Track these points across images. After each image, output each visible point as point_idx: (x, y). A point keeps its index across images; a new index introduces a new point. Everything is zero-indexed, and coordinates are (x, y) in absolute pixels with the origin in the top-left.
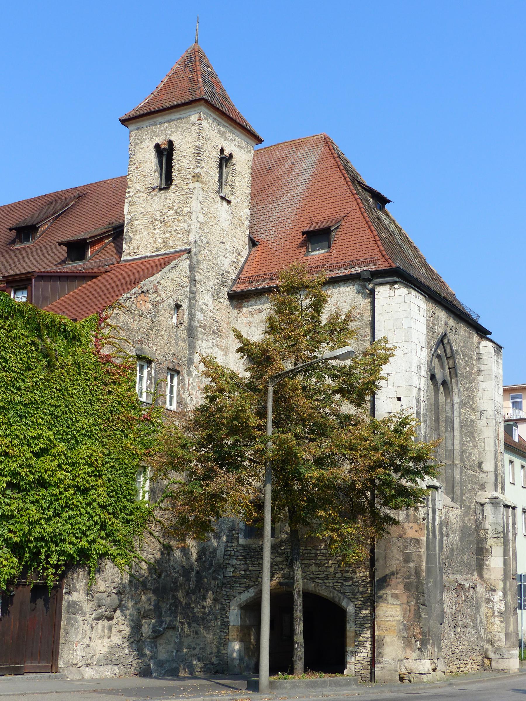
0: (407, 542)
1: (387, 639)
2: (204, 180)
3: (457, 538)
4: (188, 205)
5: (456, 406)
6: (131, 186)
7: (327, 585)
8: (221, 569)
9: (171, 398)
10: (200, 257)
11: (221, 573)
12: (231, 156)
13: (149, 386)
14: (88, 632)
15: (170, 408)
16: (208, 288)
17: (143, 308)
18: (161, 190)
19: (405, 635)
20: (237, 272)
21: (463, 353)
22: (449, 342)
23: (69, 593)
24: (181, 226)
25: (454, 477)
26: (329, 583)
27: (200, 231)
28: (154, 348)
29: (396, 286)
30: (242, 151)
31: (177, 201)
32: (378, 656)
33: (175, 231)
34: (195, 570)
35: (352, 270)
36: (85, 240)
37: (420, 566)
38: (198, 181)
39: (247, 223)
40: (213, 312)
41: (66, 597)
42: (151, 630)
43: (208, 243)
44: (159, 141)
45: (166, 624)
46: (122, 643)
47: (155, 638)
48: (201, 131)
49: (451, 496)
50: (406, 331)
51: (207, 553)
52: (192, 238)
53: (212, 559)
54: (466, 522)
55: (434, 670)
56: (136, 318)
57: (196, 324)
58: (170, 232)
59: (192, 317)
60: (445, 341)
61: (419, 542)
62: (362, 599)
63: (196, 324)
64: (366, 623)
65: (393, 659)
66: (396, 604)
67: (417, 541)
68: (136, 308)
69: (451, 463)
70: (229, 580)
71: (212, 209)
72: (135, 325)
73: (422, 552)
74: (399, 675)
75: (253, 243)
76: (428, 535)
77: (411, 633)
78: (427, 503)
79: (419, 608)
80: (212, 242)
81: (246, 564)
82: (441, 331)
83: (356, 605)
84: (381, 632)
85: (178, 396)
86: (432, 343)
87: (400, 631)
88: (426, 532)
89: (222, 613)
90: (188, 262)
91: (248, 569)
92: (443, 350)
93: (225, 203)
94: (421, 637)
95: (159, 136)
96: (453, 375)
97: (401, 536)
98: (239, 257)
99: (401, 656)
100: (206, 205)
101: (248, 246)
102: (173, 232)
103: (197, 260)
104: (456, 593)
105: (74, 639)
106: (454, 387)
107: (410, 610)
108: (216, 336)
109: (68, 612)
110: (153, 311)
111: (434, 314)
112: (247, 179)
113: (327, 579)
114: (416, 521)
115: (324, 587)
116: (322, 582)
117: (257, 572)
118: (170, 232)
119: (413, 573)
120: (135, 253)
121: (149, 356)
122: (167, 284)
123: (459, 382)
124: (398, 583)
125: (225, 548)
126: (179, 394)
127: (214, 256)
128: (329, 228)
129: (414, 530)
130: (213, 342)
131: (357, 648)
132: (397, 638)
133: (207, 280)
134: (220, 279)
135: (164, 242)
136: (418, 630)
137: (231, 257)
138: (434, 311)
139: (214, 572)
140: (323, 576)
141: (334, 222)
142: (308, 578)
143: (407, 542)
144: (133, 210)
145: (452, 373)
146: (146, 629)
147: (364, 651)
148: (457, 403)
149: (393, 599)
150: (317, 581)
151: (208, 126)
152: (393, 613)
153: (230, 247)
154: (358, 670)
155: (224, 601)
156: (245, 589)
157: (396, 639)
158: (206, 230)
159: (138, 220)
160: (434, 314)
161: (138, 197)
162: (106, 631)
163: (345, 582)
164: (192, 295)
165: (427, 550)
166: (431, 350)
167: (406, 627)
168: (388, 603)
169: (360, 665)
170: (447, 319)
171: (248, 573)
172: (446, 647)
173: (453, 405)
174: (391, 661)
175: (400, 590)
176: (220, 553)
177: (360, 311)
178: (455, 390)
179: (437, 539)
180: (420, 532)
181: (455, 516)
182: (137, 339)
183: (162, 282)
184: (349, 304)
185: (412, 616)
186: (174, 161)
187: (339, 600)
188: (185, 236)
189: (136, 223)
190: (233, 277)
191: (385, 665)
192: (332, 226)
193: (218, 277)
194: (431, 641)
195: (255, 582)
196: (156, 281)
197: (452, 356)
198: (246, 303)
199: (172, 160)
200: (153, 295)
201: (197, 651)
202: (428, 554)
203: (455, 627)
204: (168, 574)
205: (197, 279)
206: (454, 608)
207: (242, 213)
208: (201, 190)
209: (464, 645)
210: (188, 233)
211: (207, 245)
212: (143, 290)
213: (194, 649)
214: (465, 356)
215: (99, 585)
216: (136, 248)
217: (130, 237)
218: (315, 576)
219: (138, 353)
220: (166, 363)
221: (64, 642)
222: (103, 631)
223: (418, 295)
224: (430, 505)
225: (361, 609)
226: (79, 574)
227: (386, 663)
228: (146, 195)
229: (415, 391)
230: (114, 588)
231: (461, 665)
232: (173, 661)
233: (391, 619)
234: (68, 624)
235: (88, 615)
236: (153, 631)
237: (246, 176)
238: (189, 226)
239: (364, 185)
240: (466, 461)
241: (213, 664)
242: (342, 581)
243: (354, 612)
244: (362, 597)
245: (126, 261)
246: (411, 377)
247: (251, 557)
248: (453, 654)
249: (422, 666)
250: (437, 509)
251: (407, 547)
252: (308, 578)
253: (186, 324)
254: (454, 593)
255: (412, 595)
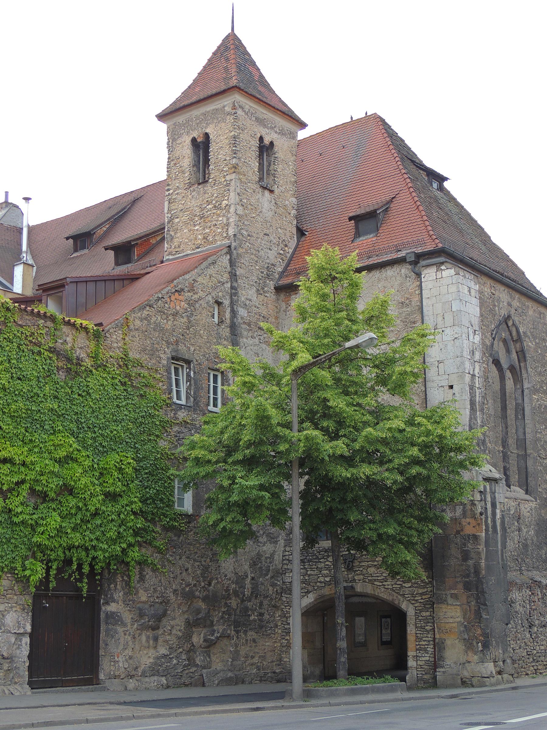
0: (465, 540)
1: (448, 642)
2: (242, 170)
3: (532, 532)
4: (226, 198)
5: (526, 392)
6: (170, 183)
7: (386, 587)
8: (279, 575)
9: (215, 399)
10: (241, 251)
11: (279, 579)
12: (272, 143)
13: (189, 388)
14: (130, 643)
15: (214, 409)
16: (252, 283)
17: (178, 308)
18: (199, 184)
19: (466, 637)
20: (284, 265)
21: (533, 335)
22: (513, 324)
23: (107, 603)
24: (220, 221)
25: (526, 468)
26: (388, 585)
27: (239, 223)
28: (192, 349)
29: (443, 267)
30: (285, 138)
31: (215, 195)
32: (439, 660)
33: (214, 226)
34: (249, 577)
35: (399, 253)
36: (129, 242)
37: (479, 564)
38: (234, 172)
39: (294, 212)
40: (258, 308)
41: (103, 608)
42: (202, 640)
43: (249, 235)
44: (195, 134)
45: (218, 632)
46: (169, 653)
47: (208, 647)
48: (236, 120)
49: (525, 488)
50: (455, 315)
51: (263, 558)
52: (231, 232)
53: (269, 564)
54: (543, 515)
55: (500, 673)
56: (170, 318)
57: (239, 321)
58: (210, 227)
59: (234, 313)
60: (510, 323)
61: (477, 539)
62: (422, 601)
63: (239, 321)
64: (427, 626)
65: (455, 663)
66: (456, 605)
67: (476, 538)
68: (169, 308)
69: (523, 453)
70: (288, 586)
71: (253, 201)
72: (169, 325)
73: (481, 549)
74: (462, 679)
75: (301, 232)
76: (487, 530)
77: (472, 634)
78: (485, 497)
79: (479, 608)
80: (254, 235)
81: (305, 568)
82: (504, 312)
83: (416, 607)
84: (442, 634)
85: (222, 397)
86: (493, 326)
87: (461, 633)
88: (484, 527)
89: (283, 619)
90: (228, 257)
91: (307, 574)
92: (508, 333)
93: (267, 193)
94: (483, 639)
95: (195, 129)
96: (522, 359)
97: (458, 532)
98: (286, 248)
99: (463, 659)
100: (245, 196)
101: (295, 236)
102: (212, 227)
103: (237, 254)
104: (530, 591)
105: (115, 650)
106: (523, 372)
107: (470, 610)
108: (262, 332)
109: (107, 623)
110: (189, 310)
111: (494, 295)
112: (291, 167)
113: (386, 581)
114: (474, 517)
115: (383, 590)
116: (381, 584)
117: (316, 577)
118: (210, 227)
119: (472, 571)
120: (177, 252)
121: (187, 358)
122: (204, 282)
123: (528, 366)
124: (457, 582)
125: (283, 553)
126: (223, 394)
127: (257, 249)
128: (375, 211)
129: (472, 525)
130: (260, 339)
131: (418, 652)
132: (458, 640)
133: (249, 273)
134: (265, 273)
135: (204, 238)
136: (479, 632)
137: (276, 249)
138: (494, 292)
139: (272, 577)
140: (382, 577)
141: (380, 205)
142: (367, 581)
143: (465, 540)
144: (173, 207)
145: (520, 356)
146: (197, 639)
147: (426, 655)
148: (528, 388)
149: (452, 600)
150: (376, 583)
151: (243, 114)
152: (453, 614)
153: (274, 238)
154: (421, 675)
155: (284, 607)
156: (304, 594)
157: (457, 642)
158: (245, 222)
159: (178, 218)
160: (494, 295)
161: (177, 194)
162: (151, 642)
163: (404, 583)
164: (233, 291)
165: (485, 547)
166: (492, 334)
167: (467, 629)
168: (447, 604)
169: (422, 670)
170: (510, 300)
171: (307, 578)
172: (520, 648)
173: (523, 391)
174: (453, 665)
175: (459, 590)
176: (278, 558)
177: (408, 296)
178: (525, 375)
179: (499, 535)
180: (477, 527)
181: (529, 509)
182: (172, 340)
183: (199, 279)
184: (396, 290)
185: (473, 616)
186: (211, 154)
187: (399, 603)
188: (225, 230)
189: (177, 220)
190: (280, 270)
191: (447, 669)
192: (378, 209)
193: (263, 270)
194: (494, 642)
195: (314, 586)
196: (192, 279)
197: (519, 339)
198: (293, 296)
199: (209, 153)
200: (189, 294)
201: (256, 660)
202: (487, 551)
203: (530, 626)
204: (218, 582)
205: (238, 273)
206: (528, 607)
207: (287, 202)
208: (239, 181)
209: (542, 645)
210: (226, 227)
211: (249, 238)
212: (177, 289)
213: (253, 657)
214: (535, 338)
215: (140, 595)
216: (177, 246)
217: (171, 235)
218: (374, 578)
219: (174, 354)
220: (206, 363)
221: (103, 654)
222: (147, 641)
223: (468, 275)
224: (489, 499)
225: (421, 611)
226: (116, 584)
227: (448, 667)
228: (185, 192)
229: (468, 378)
230: (158, 597)
231: (540, 667)
232: (229, 670)
233: (451, 620)
234: (107, 635)
235: (129, 626)
236: (205, 641)
237: (291, 164)
238: (228, 219)
239: (418, 163)
240: (540, 450)
241: (274, 673)
242: (401, 583)
243: (414, 614)
244: (422, 599)
245: (168, 260)
246: (463, 363)
247: (309, 561)
248: (529, 655)
249: (484, 670)
250: (497, 503)
251: (465, 544)
252: (367, 581)
253: (228, 321)
254: (528, 591)
255: (472, 594)
